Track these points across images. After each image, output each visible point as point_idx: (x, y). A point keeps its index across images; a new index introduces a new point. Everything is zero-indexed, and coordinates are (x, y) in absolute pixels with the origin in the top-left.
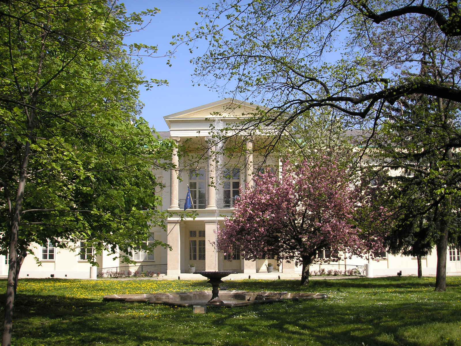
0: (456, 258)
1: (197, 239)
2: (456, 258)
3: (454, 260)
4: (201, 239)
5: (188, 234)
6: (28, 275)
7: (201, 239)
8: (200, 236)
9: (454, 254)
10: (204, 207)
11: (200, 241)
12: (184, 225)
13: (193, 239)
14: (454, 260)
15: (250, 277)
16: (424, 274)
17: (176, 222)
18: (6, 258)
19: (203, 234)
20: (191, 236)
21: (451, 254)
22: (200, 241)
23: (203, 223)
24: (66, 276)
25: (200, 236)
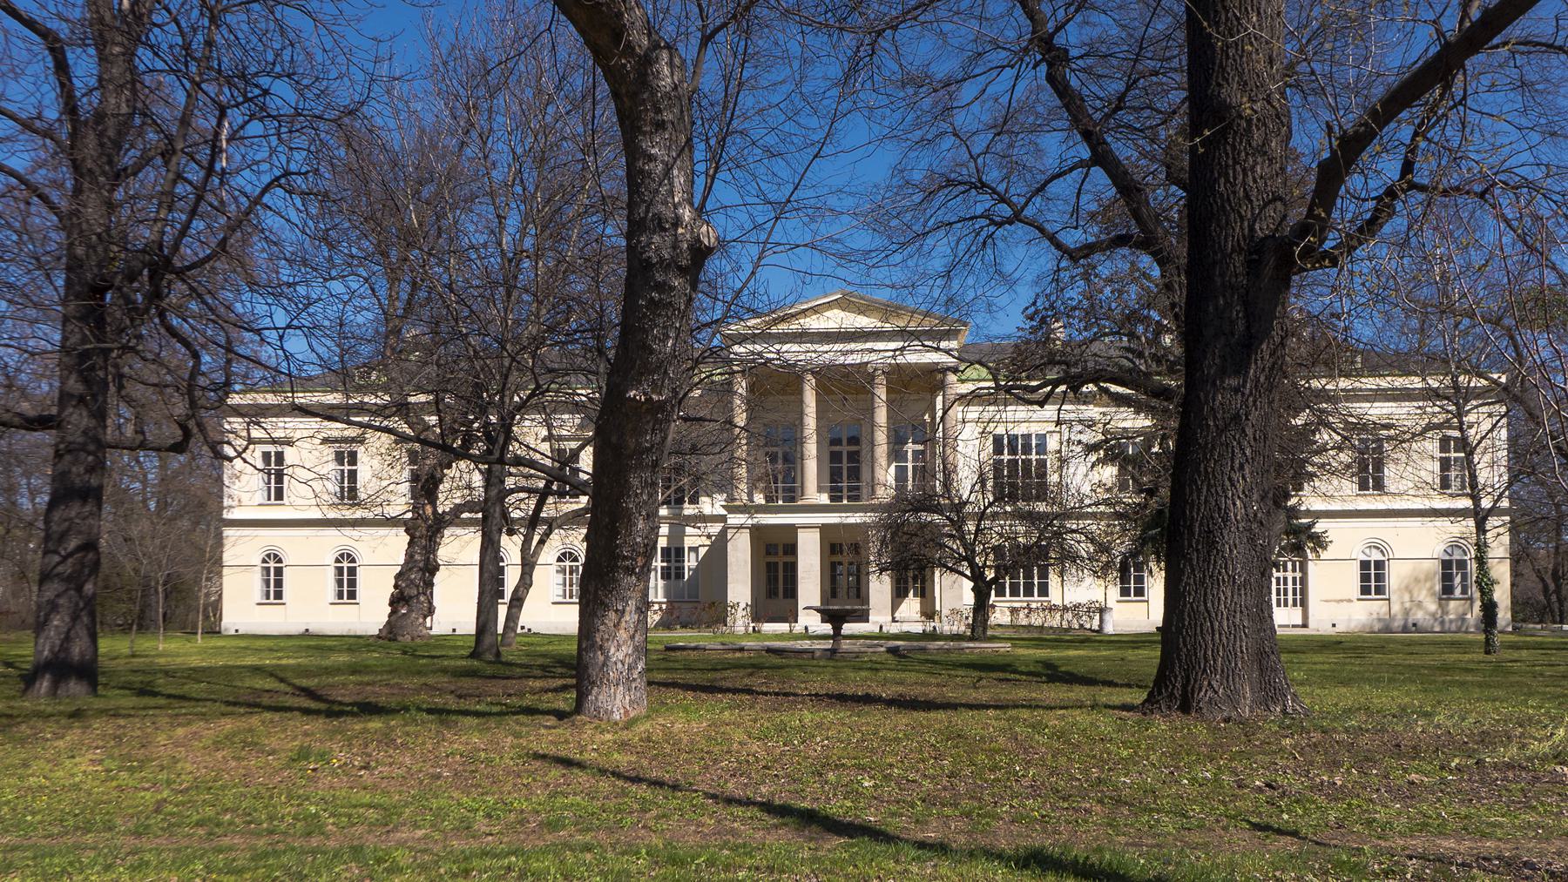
0: (1290, 602)
1: (781, 559)
2: (1290, 602)
3: (1286, 605)
4: (788, 559)
5: (763, 551)
6: (1334, 625)
7: (788, 559)
8: (785, 553)
9: (1286, 594)
10: (793, 499)
11: (785, 564)
12: (757, 532)
13: (772, 559)
14: (1286, 605)
15: (454, 630)
16: (229, 532)
17: (741, 527)
18: (1294, 626)
19: (792, 549)
20: (768, 553)
21: (1278, 594)
22: (785, 564)
23: (793, 529)
24: (1334, 625)
25: (785, 553)
